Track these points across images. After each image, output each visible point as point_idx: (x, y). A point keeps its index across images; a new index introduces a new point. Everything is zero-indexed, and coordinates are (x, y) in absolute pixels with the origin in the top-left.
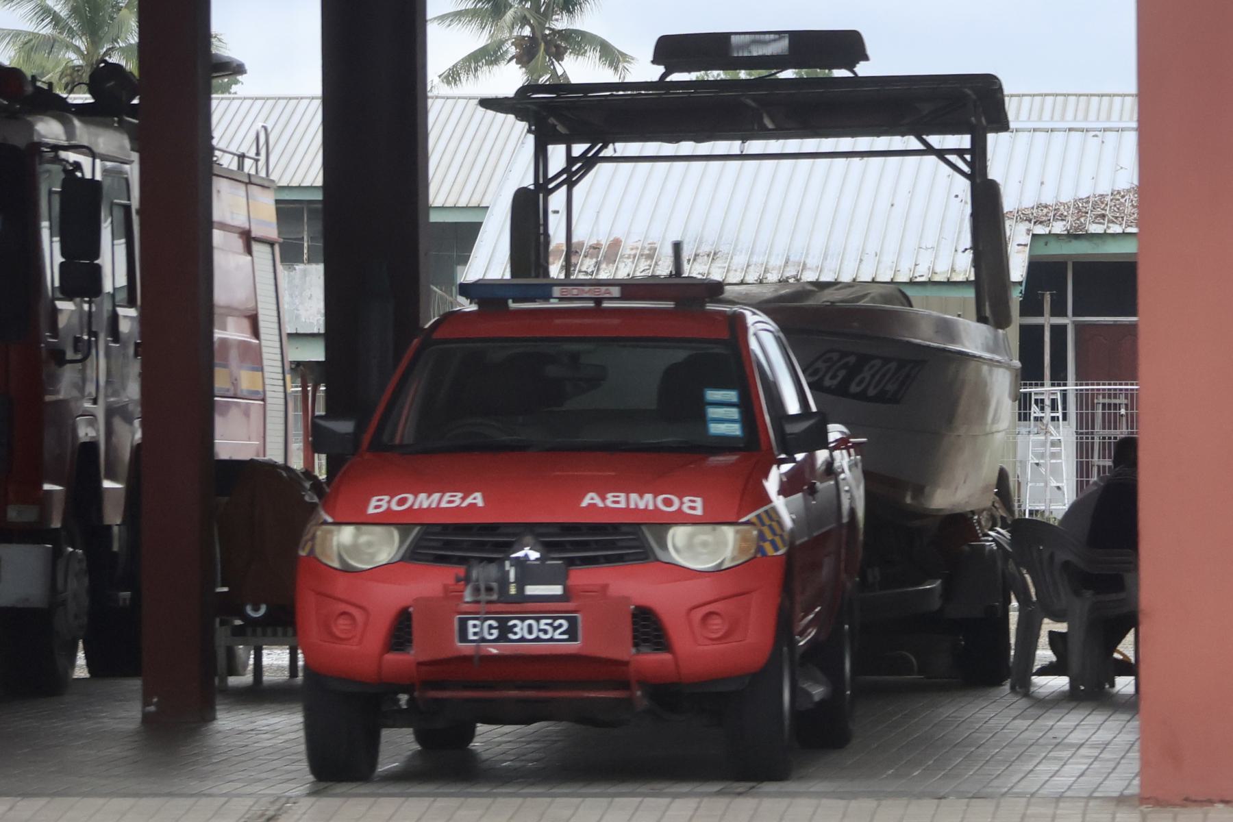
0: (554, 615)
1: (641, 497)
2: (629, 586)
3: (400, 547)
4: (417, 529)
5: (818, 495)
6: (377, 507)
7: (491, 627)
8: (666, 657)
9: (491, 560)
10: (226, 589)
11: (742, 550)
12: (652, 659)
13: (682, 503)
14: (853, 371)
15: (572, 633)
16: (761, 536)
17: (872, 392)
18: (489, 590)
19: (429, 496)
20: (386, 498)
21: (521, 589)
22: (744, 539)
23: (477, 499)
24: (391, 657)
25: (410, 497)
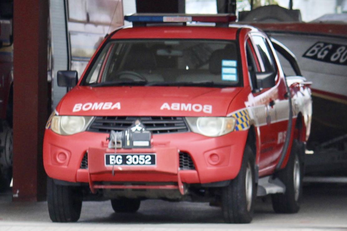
0: (145, 154)
1: (186, 105)
2: (177, 142)
3: (85, 125)
4: (92, 118)
5: (274, 106)
6: (77, 109)
7: (119, 159)
8: (194, 172)
9: (119, 131)
10: (311, 152)
11: (227, 128)
12: (187, 171)
13: (203, 108)
14: (332, 52)
15: (153, 161)
16: (237, 122)
17: (342, 61)
18: (118, 143)
19: (98, 104)
20: (81, 105)
21: (132, 142)
22: (228, 123)
23: (118, 106)
24: (80, 170)
25: (91, 104)
